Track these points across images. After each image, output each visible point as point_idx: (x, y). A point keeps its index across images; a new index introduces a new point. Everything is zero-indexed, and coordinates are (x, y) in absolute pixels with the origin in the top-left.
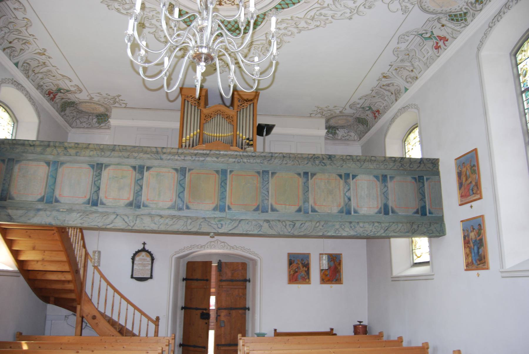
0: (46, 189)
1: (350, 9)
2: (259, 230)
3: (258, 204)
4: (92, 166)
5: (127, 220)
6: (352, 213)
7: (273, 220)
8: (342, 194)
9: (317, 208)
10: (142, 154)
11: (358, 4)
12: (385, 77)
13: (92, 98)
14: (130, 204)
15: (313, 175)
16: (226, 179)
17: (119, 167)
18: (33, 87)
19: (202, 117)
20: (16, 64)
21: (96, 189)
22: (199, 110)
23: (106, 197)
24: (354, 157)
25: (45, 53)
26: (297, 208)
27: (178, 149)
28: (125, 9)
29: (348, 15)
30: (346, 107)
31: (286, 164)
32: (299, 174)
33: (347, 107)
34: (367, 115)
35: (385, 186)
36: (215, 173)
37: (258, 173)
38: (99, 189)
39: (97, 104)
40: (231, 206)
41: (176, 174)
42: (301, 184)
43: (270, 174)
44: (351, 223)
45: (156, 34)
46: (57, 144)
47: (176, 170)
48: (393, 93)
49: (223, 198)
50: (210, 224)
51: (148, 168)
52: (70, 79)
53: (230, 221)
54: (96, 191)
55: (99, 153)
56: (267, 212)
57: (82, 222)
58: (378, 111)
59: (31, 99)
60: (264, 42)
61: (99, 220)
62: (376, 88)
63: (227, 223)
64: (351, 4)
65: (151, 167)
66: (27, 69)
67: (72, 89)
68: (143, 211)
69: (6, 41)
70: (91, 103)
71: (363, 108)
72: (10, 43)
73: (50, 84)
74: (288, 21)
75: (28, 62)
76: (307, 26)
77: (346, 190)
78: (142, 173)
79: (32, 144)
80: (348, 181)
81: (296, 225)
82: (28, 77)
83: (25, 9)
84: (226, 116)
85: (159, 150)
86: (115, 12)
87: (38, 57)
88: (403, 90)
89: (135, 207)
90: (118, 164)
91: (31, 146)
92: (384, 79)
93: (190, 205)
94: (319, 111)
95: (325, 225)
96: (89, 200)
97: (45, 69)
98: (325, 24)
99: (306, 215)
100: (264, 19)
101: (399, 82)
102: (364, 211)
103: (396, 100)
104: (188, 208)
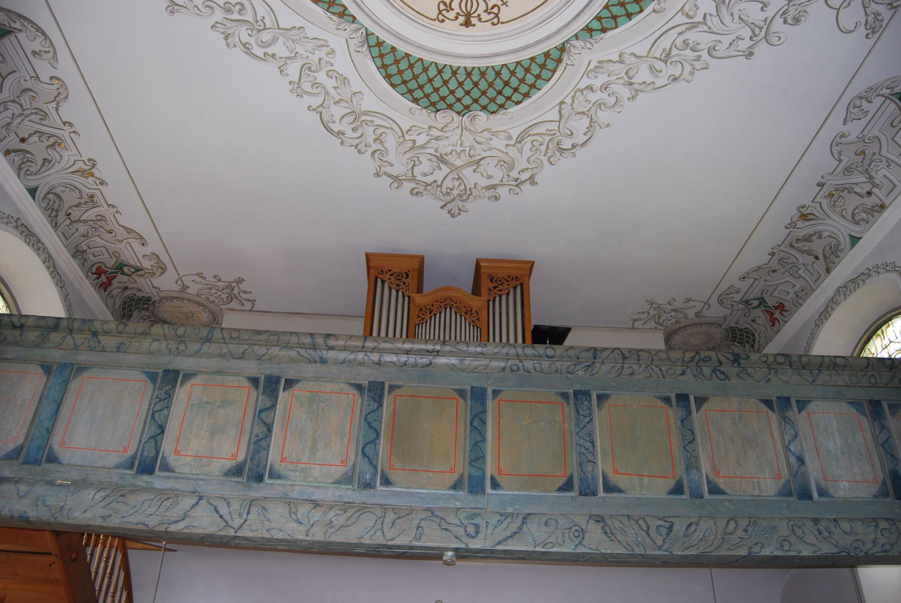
0: (30, 429)
1: (752, 26)
2: (577, 541)
3: (568, 474)
4: (153, 377)
5: (224, 511)
6: (815, 495)
7: (611, 516)
8: (780, 448)
9: (721, 483)
10: (277, 349)
11: (770, 12)
12: (804, 217)
13: (185, 287)
14: (237, 471)
15: (701, 401)
17: (219, 378)
18: (65, 250)
20: (33, 192)
21: (154, 430)
22: (407, 299)
23: (177, 452)
24: (795, 359)
25: (94, 171)
26: (671, 483)
27: (365, 339)
28: (264, 45)
29: (744, 45)
31: (632, 374)
32: (667, 400)
33: (714, 301)
34: (753, 321)
35: (883, 427)
36: (456, 396)
37: (565, 396)
38: (163, 432)
39: (196, 302)
40: (499, 479)
41: (358, 397)
42: (672, 420)
43: (594, 398)
44: (816, 521)
45: (324, 111)
46: (76, 325)
47: (359, 387)
48: (820, 256)
49: (477, 459)
50: (445, 526)
51: (290, 383)
52: (142, 238)
53: (498, 517)
54: (153, 437)
55: (172, 345)
56: (595, 494)
57: (106, 512)
58: (781, 307)
59: (49, 261)
60: (554, 126)
61: (152, 510)
62: (782, 248)
63: (493, 522)
64: (754, 13)
65: (298, 381)
66: (53, 205)
67: (147, 264)
68: (270, 488)
69: (13, 135)
70: (183, 299)
71: (747, 302)
72: (23, 140)
73: (102, 249)
75: (58, 191)
76: (653, 79)
77: (787, 438)
79: (17, 324)
80: (789, 414)
81: (676, 528)
82: (55, 226)
83: (55, 52)
84: (464, 310)
85: (320, 341)
86: (239, 52)
87: (78, 181)
88: (845, 241)
89: (248, 479)
90: (218, 372)
91: (14, 327)
92: (800, 224)
93: (392, 476)
94: (652, 313)
95: (750, 529)
96: (134, 457)
97: (91, 214)
98: (692, 73)
99: (697, 501)
100: (559, 61)
101: (840, 227)
102: (843, 490)
103: (828, 271)
104: (386, 482)
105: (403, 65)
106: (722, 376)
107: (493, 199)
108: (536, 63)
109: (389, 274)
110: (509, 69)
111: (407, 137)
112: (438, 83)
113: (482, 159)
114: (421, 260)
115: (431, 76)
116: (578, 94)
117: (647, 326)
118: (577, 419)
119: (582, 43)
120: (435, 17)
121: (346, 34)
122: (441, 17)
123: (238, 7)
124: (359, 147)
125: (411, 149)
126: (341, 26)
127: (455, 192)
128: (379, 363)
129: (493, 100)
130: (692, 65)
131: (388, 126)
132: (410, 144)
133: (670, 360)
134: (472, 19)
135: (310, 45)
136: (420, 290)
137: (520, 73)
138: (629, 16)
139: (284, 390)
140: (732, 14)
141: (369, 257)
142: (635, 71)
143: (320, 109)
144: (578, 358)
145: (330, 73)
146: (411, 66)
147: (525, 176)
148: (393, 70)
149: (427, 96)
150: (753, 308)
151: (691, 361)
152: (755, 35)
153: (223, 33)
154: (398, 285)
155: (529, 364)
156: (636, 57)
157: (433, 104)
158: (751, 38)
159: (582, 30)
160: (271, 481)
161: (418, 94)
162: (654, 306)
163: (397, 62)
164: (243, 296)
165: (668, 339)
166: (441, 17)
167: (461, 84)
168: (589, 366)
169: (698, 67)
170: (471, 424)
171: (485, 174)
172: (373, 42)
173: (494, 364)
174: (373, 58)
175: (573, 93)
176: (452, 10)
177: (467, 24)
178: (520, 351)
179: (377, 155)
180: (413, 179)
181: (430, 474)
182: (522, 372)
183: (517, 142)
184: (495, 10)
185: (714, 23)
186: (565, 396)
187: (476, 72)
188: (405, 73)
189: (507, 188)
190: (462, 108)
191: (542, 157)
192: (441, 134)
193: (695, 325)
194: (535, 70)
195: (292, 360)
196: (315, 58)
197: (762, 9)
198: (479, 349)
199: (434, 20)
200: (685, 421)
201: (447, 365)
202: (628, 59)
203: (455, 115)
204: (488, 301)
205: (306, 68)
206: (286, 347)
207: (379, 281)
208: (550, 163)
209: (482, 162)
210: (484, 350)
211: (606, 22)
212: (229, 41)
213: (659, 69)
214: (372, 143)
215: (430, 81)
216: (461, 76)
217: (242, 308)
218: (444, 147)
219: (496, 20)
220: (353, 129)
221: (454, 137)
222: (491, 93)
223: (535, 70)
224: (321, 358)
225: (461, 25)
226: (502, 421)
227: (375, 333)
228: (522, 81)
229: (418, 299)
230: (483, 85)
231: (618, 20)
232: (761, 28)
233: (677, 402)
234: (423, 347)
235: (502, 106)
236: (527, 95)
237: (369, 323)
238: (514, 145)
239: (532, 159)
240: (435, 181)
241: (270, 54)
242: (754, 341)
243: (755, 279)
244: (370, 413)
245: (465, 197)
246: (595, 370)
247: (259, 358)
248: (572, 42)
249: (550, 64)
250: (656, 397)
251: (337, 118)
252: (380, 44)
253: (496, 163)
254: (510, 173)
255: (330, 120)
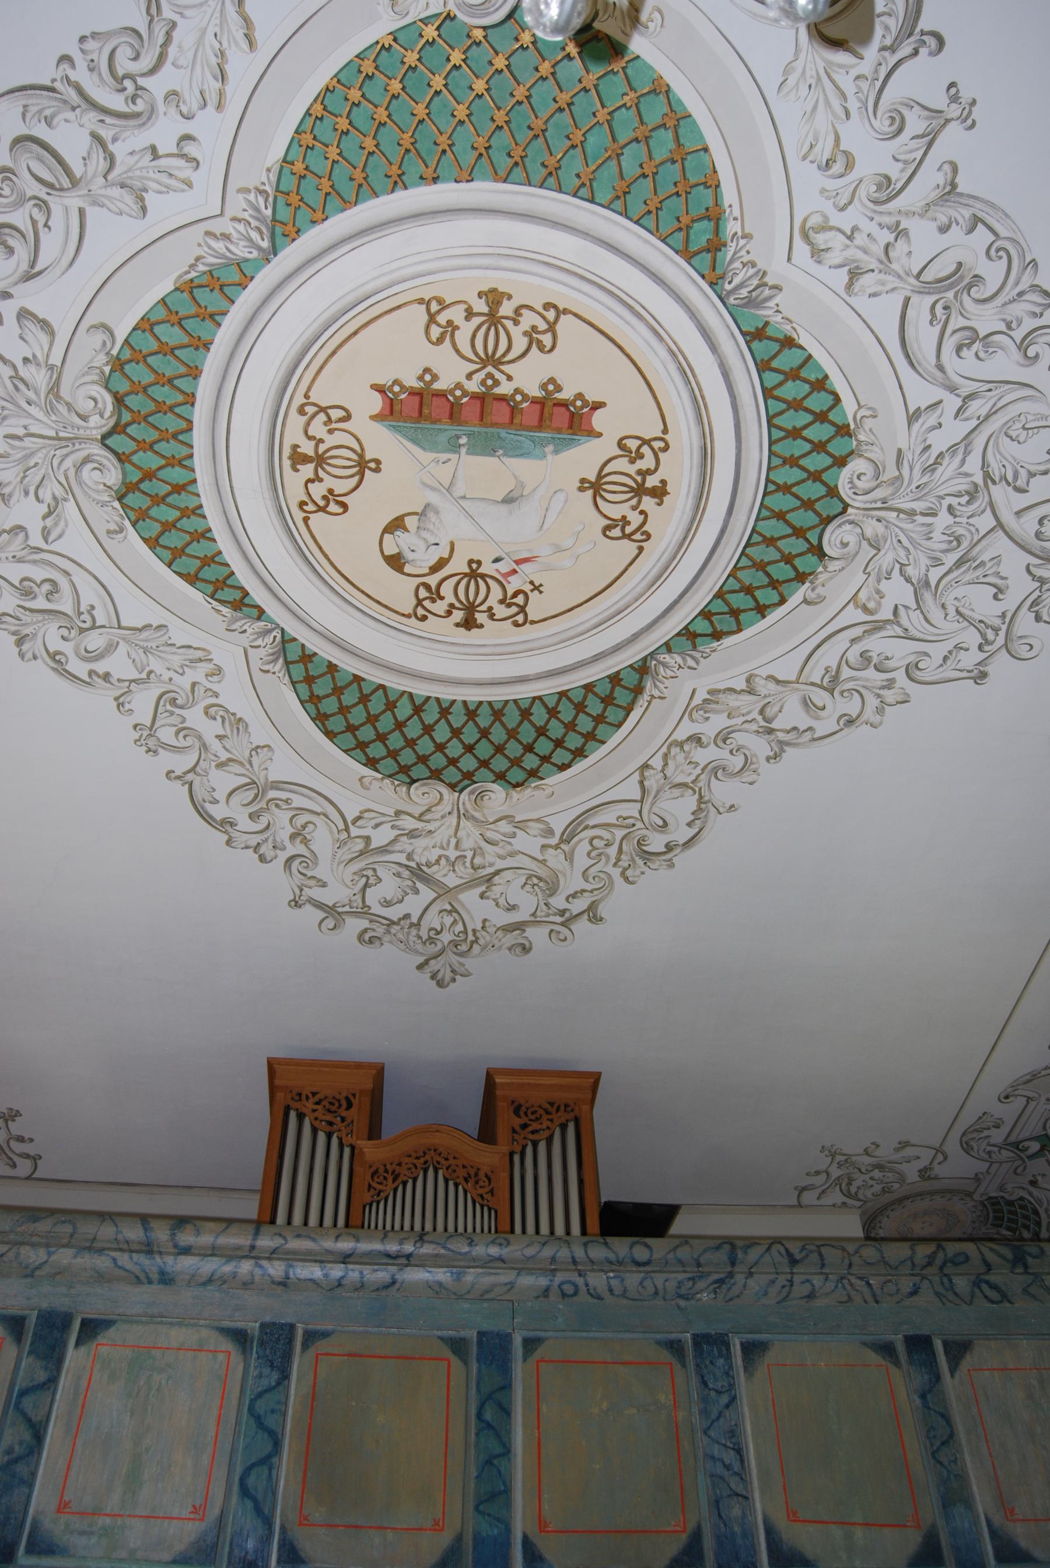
1: (980, 625)
3: (691, 1526)
10: (69, 1252)
11: (1009, 603)
15: (958, 1350)
16: (507, 1387)
19: (356, 1180)
22: (347, 1151)
28: (89, 656)
29: (970, 659)
30: (948, 1148)
31: (811, 1296)
32: (887, 1350)
33: (953, 1146)
36: (447, 1353)
37: (675, 1347)
41: (236, 1358)
47: (240, 1337)
49: (493, 1496)
51: (91, 1328)
60: (632, 810)
65: (108, 1324)
71: (1016, 1145)
74: (733, 701)
78: (50, 1352)
84: (462, 1173)
86: (42, 669)
94: (835, 1172)
98: (880, 711)
100: (638, 690)
105: (350, 697)
106: (993, 1294)
107: (518, 950)
108: (595, 694)
109: (312, 1100)
110: (546, 706)
111: (354, 831)
112: (413, 729)
113: (497, 872)
114: (378, 1072)
115: (401, 718)
116: (675, 750)
117: (828, 1200)
118: (704, 1400)
119: (678, 659)
120: (409, 610)
121: (245, 640)
122: (420, 612)
123: (46, 587)
124: (263, 850)
125: (362, 853)
126: (236, 626)
127: (446, 937)
128: (284, 1283)
129: (516, 762)
130: (878, 696)
131: (319, 810)
132: (360, 845)
133: (886, 1264)
134: (477, 615)
135: (176, 658)
136: (374, 1132)
137: (567, 712)
138: (762, 610)
139: (78, 1344)
140: (943, 606)
141: (273, 1067)
142: (776, 709)
143: (190, 777)
144: (699, 1265)
145: (212, 711)
146: (364, 699)
147: (579, 905)
148: (330, 705)
149: (393, 754)
150: (1031, 1157)
151: (929, 1264)
152: (988, 643)
153: (14, 633)
154: (331, 1124)
155: (598, 1281)
156: (778, 682)
157: (404, 769)
158: (980, 648)
159: (678, 634)
160: (32, 1560)
161: (376, 750)
162: (839, 1158)
163: (338, 691)
164: (16, 1146)
165: (870, 1222)
166: (420, 612)
167: (456, 733)
168: (721, 1281)
169: (890, 700)
170: (479, 1416)
171: (502, 901)
172: (294, 653)
173: (527, 1281)
174: (293, 683)
175: (664, 749)
176: (442, 598)
177: (469, 623)
178: (579, 1253)
179: (295, 864)
180: (364, 911)
181: (390, 1535)
182: (583, 1297)
183: (562, 840)
184: (520, 600)
185: (913, 620)
186: (675, 1347)
187: (485, 710)
188: (352, 711)
189: (544, 930)
190: (459, 777)
191: (610, 869)
192: (419, 825)
193: (921, 1194)
194: (594, 707)
195: (101, 1278)
196: (185, 682)
197: (995, 597)
198: (494, 1251)
199: (409, 616)
200: (930, 1393)
201: (428, 1285)
202: (764, 687)
203: (445, 791)
204: (511, 1154)
205: (168, 700)
206: (89, 1249)
207: (293, 1115)
208: (627, 879)
209: (496, 879)
210: (505, 1252)
211: (721, 622)
212: (25, 647)
213: (820, 704)
214: (287, 843)
215: (400, 726)
216: (457, 719)
217: (10, 1172)
218: (424, 850)
219: (521, 617)
220: (251, 816)
221: (444, 831)
222: (514, 749)
223: (594, 707)
224: (162, 1273)
225: (457, 625)
226: (544, 1409)
227: (281, 1218)
228: (571, 726)
229: (370, 1150)
230: (498, 734)
231: (742, 617)
232: (996, 630)
233: (909, 1353)
234: (377, 1246)
235: (533, 774)
236: (579, 753)
237: (269, 1201)
238: (557, 847)
239: (592, 871)
240: (407, 916)
241: (101, 673)
242: (1039, 1224)
243: (1029, 1099)
244: (260, 1395)
245: (464, 947)
246: (735, 1291)
247: (30, 1273)
248: (661, 657)
249: (622, 697)
250: (864, 1344)
251: (221, 795)
252: (307, 657)
253: (523, 880)
254: (552, 901)
255: (208, 798)
